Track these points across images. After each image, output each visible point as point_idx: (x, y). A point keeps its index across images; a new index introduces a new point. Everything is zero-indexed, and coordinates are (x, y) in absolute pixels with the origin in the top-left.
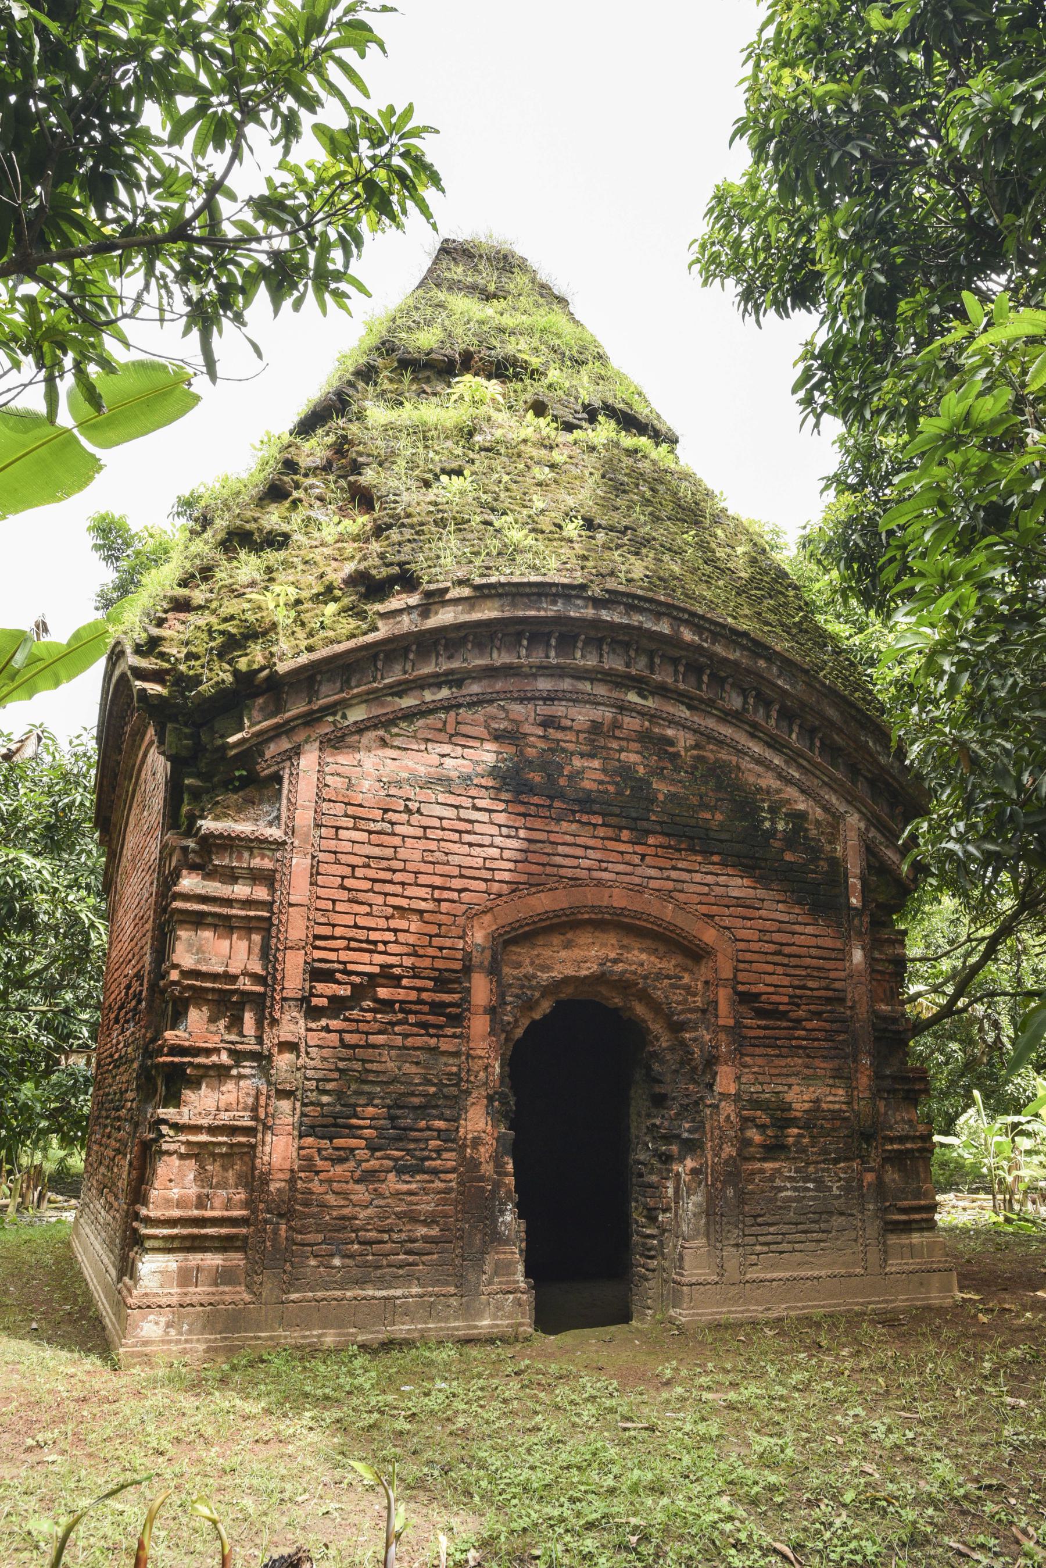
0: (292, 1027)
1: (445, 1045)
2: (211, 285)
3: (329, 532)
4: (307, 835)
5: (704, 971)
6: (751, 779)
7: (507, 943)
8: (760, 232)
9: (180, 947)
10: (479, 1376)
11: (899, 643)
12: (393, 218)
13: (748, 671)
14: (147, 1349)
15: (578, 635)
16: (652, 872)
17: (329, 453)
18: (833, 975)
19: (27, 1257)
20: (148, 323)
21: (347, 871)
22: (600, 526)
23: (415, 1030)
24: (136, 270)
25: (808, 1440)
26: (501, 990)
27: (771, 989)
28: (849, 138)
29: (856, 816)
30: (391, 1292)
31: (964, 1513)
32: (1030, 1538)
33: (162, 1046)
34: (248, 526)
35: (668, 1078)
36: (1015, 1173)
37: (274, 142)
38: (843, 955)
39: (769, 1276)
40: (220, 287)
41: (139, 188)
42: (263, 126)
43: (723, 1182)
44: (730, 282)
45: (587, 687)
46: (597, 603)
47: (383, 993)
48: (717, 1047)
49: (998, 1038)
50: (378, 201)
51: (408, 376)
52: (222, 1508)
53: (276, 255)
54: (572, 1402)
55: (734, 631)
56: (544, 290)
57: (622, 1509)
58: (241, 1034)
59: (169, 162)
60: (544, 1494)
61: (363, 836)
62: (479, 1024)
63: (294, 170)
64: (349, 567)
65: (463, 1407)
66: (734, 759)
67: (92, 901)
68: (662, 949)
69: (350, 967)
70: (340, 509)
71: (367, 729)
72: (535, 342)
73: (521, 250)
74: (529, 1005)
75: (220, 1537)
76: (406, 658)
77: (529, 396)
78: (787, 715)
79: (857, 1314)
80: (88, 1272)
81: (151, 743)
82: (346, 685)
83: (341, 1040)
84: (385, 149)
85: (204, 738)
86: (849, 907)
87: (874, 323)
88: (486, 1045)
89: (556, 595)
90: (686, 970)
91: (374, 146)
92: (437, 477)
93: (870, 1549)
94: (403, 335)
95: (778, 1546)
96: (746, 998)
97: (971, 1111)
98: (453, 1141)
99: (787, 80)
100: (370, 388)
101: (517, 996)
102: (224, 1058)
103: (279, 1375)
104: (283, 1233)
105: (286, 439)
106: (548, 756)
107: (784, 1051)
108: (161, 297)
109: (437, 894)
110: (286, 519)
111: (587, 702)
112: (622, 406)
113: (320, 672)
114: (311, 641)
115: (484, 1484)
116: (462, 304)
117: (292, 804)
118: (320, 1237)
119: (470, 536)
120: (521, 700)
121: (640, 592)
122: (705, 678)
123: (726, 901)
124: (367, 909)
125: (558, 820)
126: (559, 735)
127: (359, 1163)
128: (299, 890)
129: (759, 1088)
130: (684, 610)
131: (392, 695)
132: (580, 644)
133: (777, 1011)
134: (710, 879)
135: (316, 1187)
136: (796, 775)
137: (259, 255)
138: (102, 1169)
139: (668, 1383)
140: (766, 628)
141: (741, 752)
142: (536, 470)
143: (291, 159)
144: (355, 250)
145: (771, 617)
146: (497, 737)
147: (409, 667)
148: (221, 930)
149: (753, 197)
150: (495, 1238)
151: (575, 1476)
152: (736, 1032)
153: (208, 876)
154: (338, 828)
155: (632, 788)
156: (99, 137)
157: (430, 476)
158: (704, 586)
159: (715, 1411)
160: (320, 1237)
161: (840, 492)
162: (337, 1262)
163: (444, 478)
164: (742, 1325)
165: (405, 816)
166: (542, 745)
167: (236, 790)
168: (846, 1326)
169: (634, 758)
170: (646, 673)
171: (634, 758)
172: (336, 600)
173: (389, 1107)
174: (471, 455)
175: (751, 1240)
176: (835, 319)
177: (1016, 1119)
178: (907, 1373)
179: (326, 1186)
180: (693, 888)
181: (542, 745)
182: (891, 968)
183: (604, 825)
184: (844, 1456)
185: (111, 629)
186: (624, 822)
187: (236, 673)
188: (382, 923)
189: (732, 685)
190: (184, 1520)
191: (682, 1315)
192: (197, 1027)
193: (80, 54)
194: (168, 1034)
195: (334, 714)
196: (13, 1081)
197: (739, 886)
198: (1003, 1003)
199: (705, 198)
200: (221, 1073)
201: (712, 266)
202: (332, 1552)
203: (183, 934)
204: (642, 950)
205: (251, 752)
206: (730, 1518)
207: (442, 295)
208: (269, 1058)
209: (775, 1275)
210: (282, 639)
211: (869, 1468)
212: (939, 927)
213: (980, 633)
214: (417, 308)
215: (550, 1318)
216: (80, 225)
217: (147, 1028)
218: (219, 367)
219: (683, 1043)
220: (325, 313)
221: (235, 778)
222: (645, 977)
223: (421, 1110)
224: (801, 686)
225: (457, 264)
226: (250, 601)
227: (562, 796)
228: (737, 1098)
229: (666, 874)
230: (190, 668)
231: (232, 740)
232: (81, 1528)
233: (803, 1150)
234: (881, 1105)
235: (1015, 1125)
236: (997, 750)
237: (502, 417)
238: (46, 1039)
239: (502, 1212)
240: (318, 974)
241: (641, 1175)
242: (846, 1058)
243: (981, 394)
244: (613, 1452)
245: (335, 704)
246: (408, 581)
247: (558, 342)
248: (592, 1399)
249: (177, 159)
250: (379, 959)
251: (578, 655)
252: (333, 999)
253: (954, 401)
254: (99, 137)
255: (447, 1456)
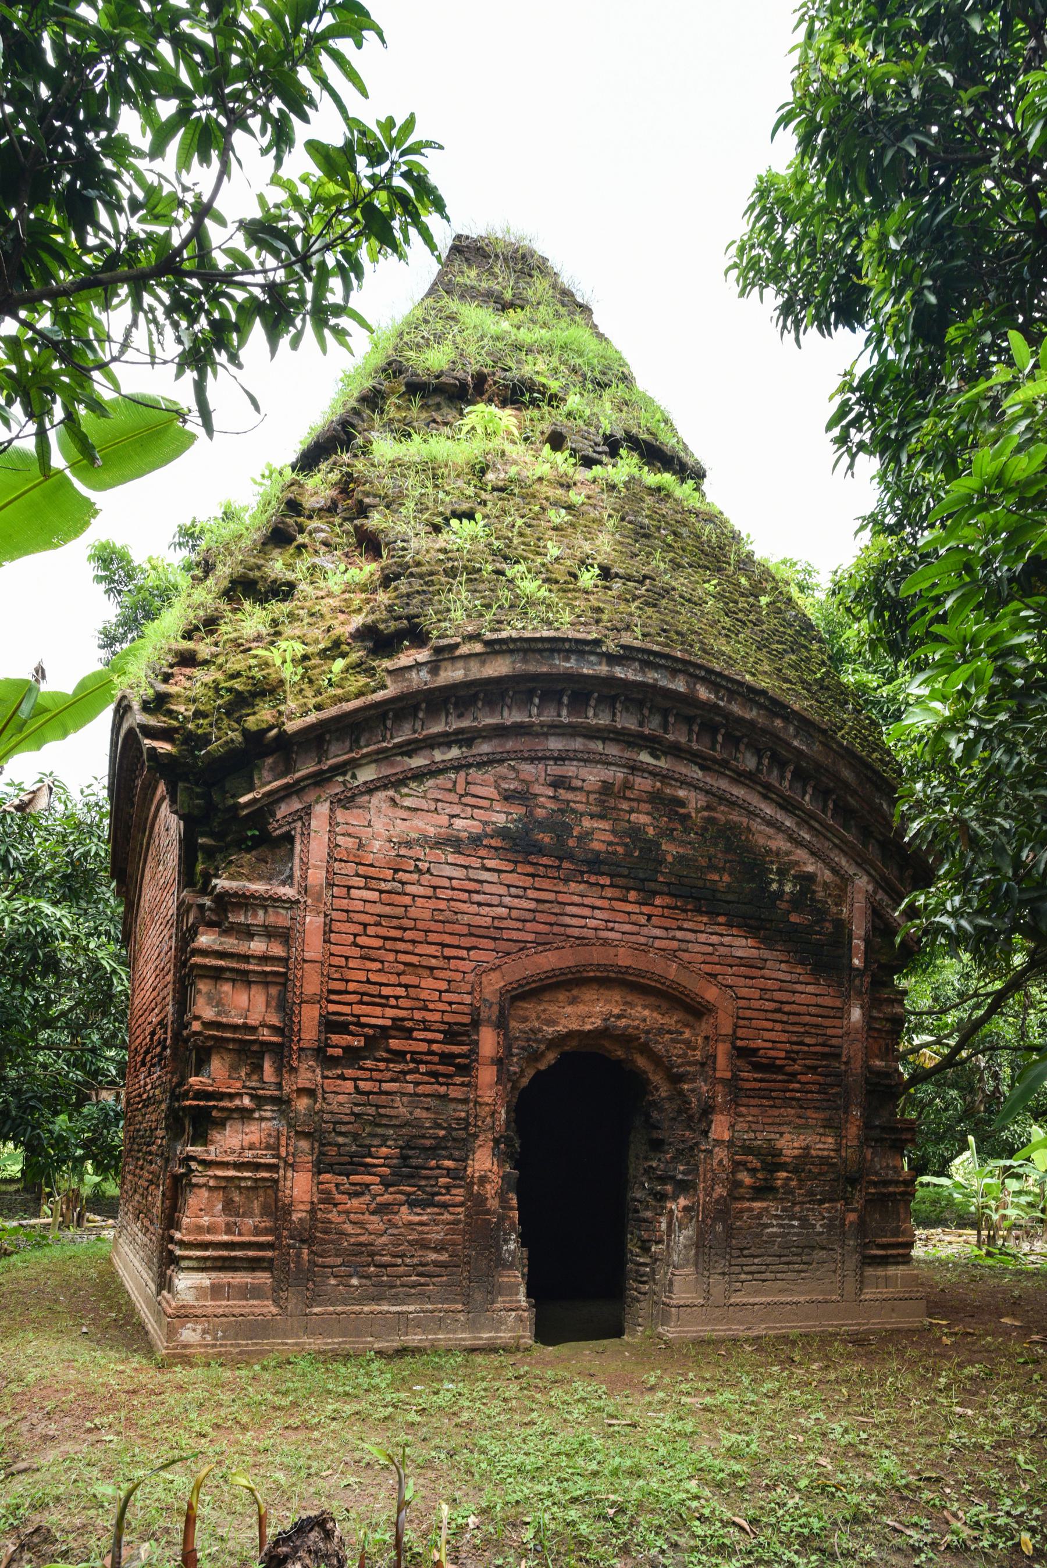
0: (309, 1075)
1: (455, 1093)
2: (203, 321)
3: (335, 582)
4: (320, 894)
5: (705, 1027)
6: (761, 841)
7: (515, 999)
8: (804, 234)
9: (201, 1001)
10: (483, 1379)
11: (922, 706)
12: (395, 248)
13: (764, 731)
14: (188, 1351)
15: (591, 693)
16: (658, 932)
17: (333, 493)
18: (829, 1032)
19: (74, 1271)
20: (138, 354)
21: (359, 929)
22: (617, 575)
23: (426, 1078)
24: (123, 302)
25: (772, 1438)
26: (507, 1042)
27: (769, 1045)
28: (906, 131)
29: (865, 878)
30: (405, 1308)
31: (903, 1498)
32: (958, 1519)
33: (187, 1091)
34: (251, 574)
35: (666, 1125)
36: (1002, 1212)
37: (264, 152)
38: (842, 1013)
39: (751, 1300)
40: (212, 323)
41: (121, 210)
42: (251, 132)
43: (714, 1219)
44: (770, 291)
45: (598, 746)
46: (611, 659)
47: (394, 1044)
48: (713, 1098)
49: (997, 1088)
50: (378, 228)
51: (418, 402)
52: (258, 1479)
53: (271, 288)
54: (564, 1402)
55: (751, 689)
56: (566, 297)
57: (602, 1488)
58: (261, 1080)
59: (151, 179)
60: (536, 1474)
61: (373, 896)
62: (487, 1075)
63: (287, 185)
64: (358, 621)
65: (467, 1404)
66: (745, 820)
67: (113, 948)
68: (665, 1006)
69: (363, 1020)
70: (346, 555)
71: (377, 789)
72: (555, 362)
73: (541, 248)
74: (535, 1057)
75: (256, 1502)
76: (416, 716)
77: (546, 427)
78: (801, 776)
79: (831, 1335)
80: (129, 1285)
81: (163, 799)
82: (355, 744)
83: (356, 1087)
84: (383, 169)
85: (216, 798)
86: (851, 967)
87: (920, 350)
88: (493, 1093)
89: (570, 651)
90: (687, 1026)
91: (372, 164)
92: (447, 520)
93: (816, 1524)
94: (411, 354)
95: (737, 1519)
96: (744, 1053)
97: (967, 1154)
98: (462, 1179)
99: (840, 59)
100: (376, 416)
101: (523, 1048)
102: (247, 1101)
103: (304, 1375)
104: (305, 1257)
105: (289, 475)
106: (559, 817)
107: (778, 1102)
108: (150, 334)
109: (448, 952)
110: (291, 567)
111: (598, 762)
112: (645, 436)
113: (329, 732)
114: (319, 699)
115: (484, 1466)
116: (477, 316)
117: (305, 865)
118: (339, 1261)
119: (481, 587)
120: (532, 760)
121: (656, 648)
122: (720, 738)
123: (730, 961)
124: (379, 966)
125: (566, 881)
126: (569, 796)
127: (374, 1197)
128: (314, 948)
129: (752, 1135)
130: (701, 667)
131: (402, 754)
132: (593, 703)
133: (773, 1065)
134: (714, 939)
135: (334, 1216)
136: (807, 837)
137: (252, 287)
138: (137, 1197)
139: (652, 1389)
140: (786, 686)
141: (752, 814)
142: (552, 513)
143: (284, 173)
144: (355, 282)
145: (791, 674)
146: (508, 797)
147: (418, 726)
148: (238, 985)
149: (798, 194)
150: (501, 1264)
151: (564, 1461)
152: (733, 1085)
153: (226, 932)
154: (349, 888)
155: (641, 850)
156: (74, 148)
157: (438, 520)
158: (723, 640)
159: (692, 1412)
160: (339, 1261)
161: (875, 533)
162: (355, 1281)
163: (454, 523)
164: (723, 1341)
165: (416, 876)
166: (552, 805)
167: (248, 850)
168: (818, 1344)
169: (644, 819)
170: (660, 732)
171: (644, 819)
172: (344, 655)
173: (401, 1148)
174: (484, 495)
175: (737, 1269)
176: (880, 341)
177: (1008, 1163)
178: (868, 1385)
179: (343, 1217)
180: (697, 948)
181: (552, 805)
182: (888, 1026)
183: (612, 886)
184: (802, 1451)
185: (116, 680)
186: (631, 883)
187: (245, 732)
188: (393, 979)
189: (748, 746)
190: (226, 1488)
191: (670, 1332)
192: (217, 1073)
193: (46, 44)
194: (192, 1080)
195: (344, 774)
196: (47, 1114)
197: (743, 946)
198: (1004, 1057)
199: (745, 193)
200: (245, 1115)
201: (754, 274)
202: (353, 1515)
203: (203, 986)
204: (645, 1007)
205: (263, 811)
206: (697, 1497)
207: (453, 305)
208: (288, 1102)
209: (757, 1300)
210: (290, 697)
211: (823, 1461)
212: (942, 986)
213: (991, 710)
214: (426, 321)
215: (549, 1331)
216: (61, 257)
217: (173, 1073)
218: (215, 417)
219: (681, 1093)
220: (324, 351)
221: (248, 838)
222: (647, 1032)
223: (432, 1151)
224: (817, 747)
225: (470, 266)
226: (255, 657)
227: (570, 857)
228: (731, 1144)
229: (671, 934)
230: (198, 726)
231: (243, 800)
232: (138, 1493)
233: (791, 1192)
234: (869, 1153)
235: (1007, 1169)
236: (996, 828)
237: (516, 451)
238: (77, 1075)
239: (506, 1242)
240: (331, 1025)
241: (637, 1211)
242: (837, 1109)
243: (1019, 449)
244: (598, 1443)
245: (345, 763)
246: (417, 636)
247: (579, 361)
248: (583, 1400)
249: (160, 175)
250: (390, 1012)
251: (591, 713)
252: (348, 1049)
253: (988, 458)
254: (74, 148)
255: (453, 1444)
